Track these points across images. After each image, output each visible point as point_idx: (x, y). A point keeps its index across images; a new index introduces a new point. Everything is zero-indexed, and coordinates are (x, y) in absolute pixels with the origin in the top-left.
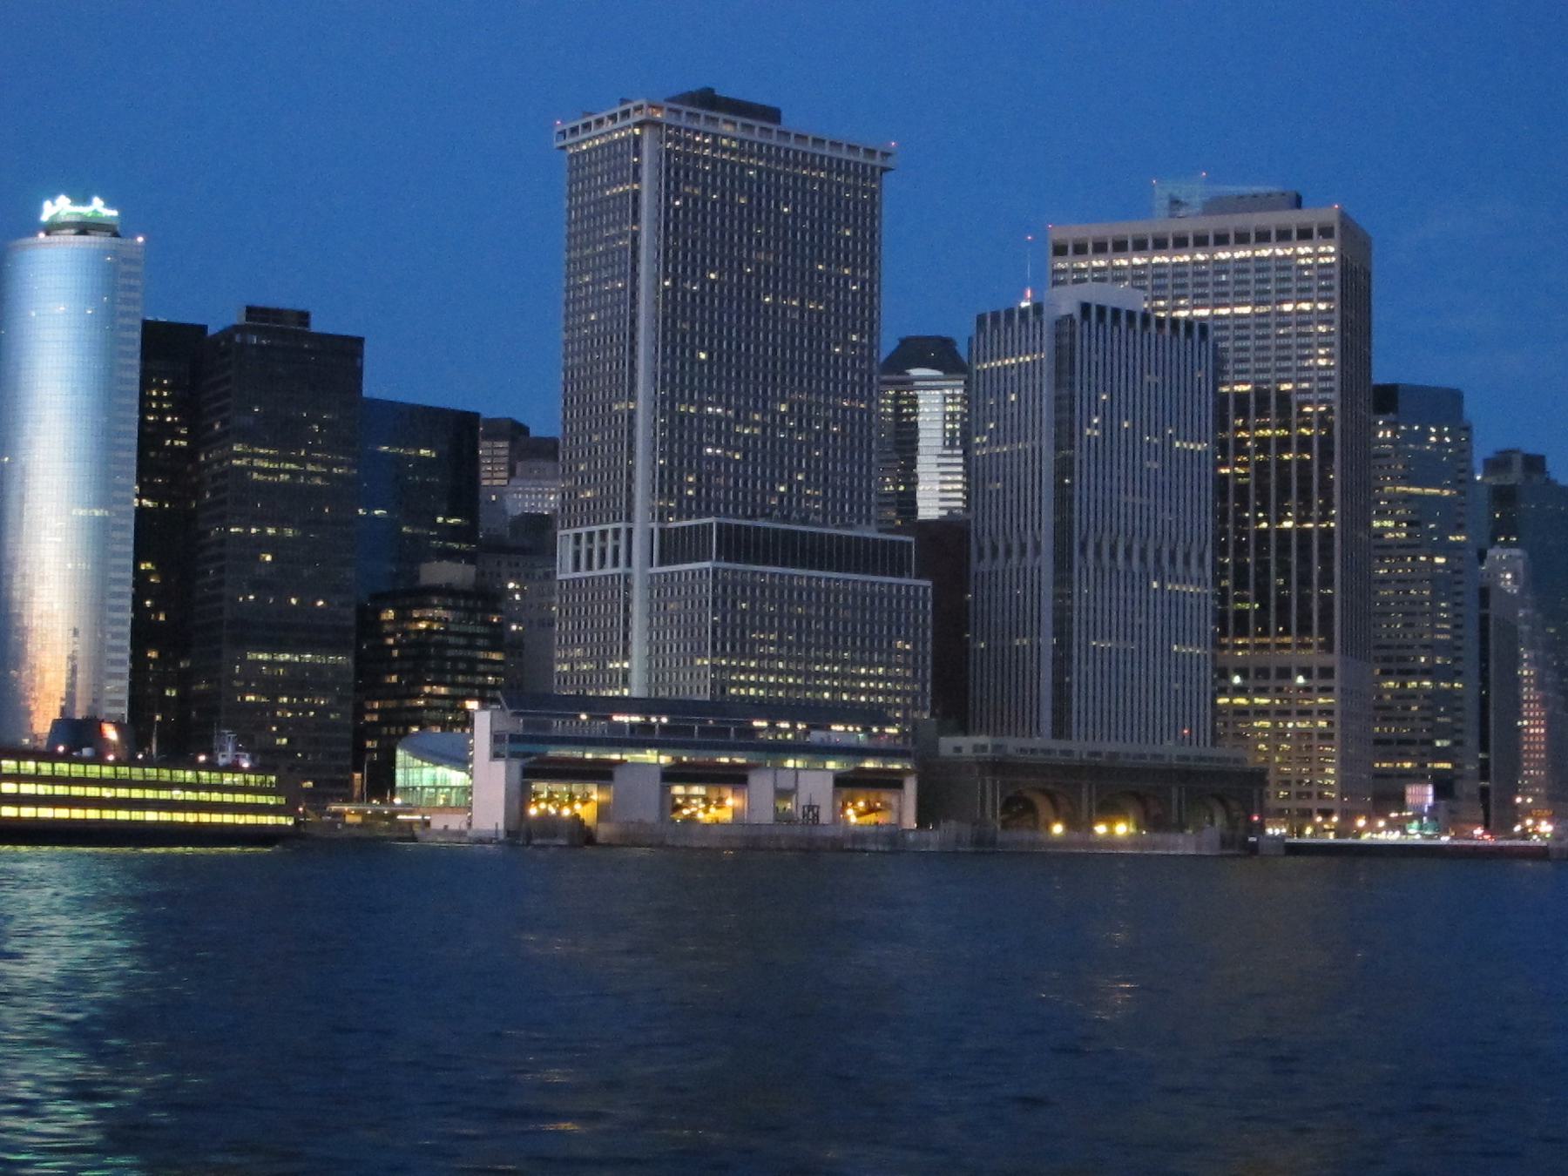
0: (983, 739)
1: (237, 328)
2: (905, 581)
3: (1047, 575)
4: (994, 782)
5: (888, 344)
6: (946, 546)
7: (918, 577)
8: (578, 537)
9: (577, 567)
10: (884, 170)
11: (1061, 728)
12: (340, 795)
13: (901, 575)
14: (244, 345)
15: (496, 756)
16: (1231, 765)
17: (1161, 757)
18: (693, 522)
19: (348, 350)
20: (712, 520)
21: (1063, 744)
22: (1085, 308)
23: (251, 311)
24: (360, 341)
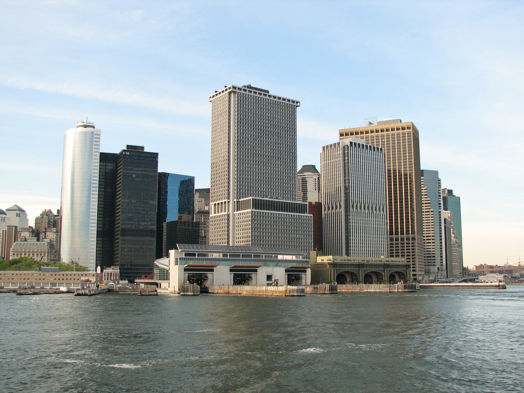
0: (331, 257)
1: (123, 150)
2: (305, 215)
3: (343, 214)
4: (334, 270)
5: (299, 168)
6: (316, 208)
7: (309, 214)
8: (215, 205)
9: (215, 213)
10: (297, 106)
11: (348, 254)
12: (139, 277)
13: (304, 213)
14: (125, 155)
15: (176, 264)
16: (352, 262)
17: (382, 261)
18: (244, 199)
19: (154, 157)
20: (251, 198)
21: (349, 258)
22: (351, 143)
23: (128, 146)
24: (157, 154)
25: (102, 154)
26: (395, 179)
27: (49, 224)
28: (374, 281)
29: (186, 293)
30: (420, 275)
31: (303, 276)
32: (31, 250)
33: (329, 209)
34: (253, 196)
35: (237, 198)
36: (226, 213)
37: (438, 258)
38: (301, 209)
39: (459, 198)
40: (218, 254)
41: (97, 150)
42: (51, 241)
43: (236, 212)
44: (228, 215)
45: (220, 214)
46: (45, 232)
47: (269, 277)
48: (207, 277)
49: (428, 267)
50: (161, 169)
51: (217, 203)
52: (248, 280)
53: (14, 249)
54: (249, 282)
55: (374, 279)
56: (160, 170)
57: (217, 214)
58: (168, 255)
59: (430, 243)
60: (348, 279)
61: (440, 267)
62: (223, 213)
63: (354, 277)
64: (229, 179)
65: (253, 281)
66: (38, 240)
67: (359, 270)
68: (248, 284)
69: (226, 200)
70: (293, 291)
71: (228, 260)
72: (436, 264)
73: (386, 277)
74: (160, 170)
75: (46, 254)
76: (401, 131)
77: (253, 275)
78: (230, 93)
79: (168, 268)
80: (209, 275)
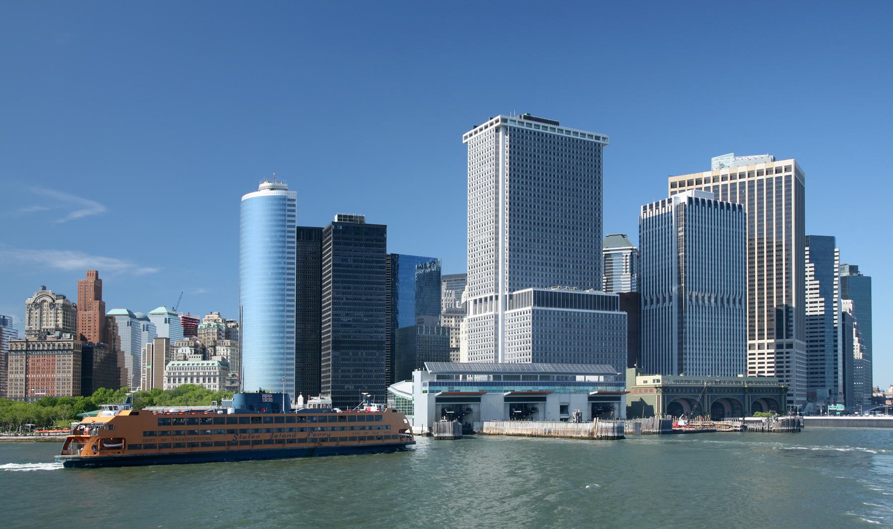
2: (616, 312)
3: (675, 310)
8: (475, 301)
9: (475, 313)
13: (614, 310)
19: (380, 231)
20: (531, 289)
22: (690, 199)
25: (300, 230)
26: (770, 252)
27: (219, 334)
28: (726, 412)
29: (442, 435)
30: (798, 402)
31: (616, 406)
32: (189, 374)
33: (652, 303)
34: (534, 286)
35: (510, 290)
36: (493, 313)
37: (829, 375)
38: (607, 303)
39: (869, 279)
40: (486, 376)
41: (292, 224)
42: (223, 359)
43: (508, 312)
44: (496, 316)
45: (483, 314)
46: (214, 347)
47: (564, 409)
48: (470, 410)
49: (812, 389)
50: (391, 248)
51: (478, 298)
52: (532, 413)
53: (169, 373)
54: (534, 415)
55: (686, 407)
56: (389, 252)
57: (478, 316)
58: (409, 378)
59: (817, 351)
60: (727, 409)
61: (832, 388)
62: (488, 313)
63: (736, 406)
64: (497, 261)
65: (541, 414)
66: (204, 358)
67: (744, 396)
68: (537, 420)
69: (493, 294)
70: (607, 430)
71: (502, 384)
72: (828, 384)
73: (707, 406)
74: (389, 252)
75: (217, 379)
76: (738, 181)
77: (539, 405)
78: (497, 130)
79: (410, 397)
80: (473, 406)
